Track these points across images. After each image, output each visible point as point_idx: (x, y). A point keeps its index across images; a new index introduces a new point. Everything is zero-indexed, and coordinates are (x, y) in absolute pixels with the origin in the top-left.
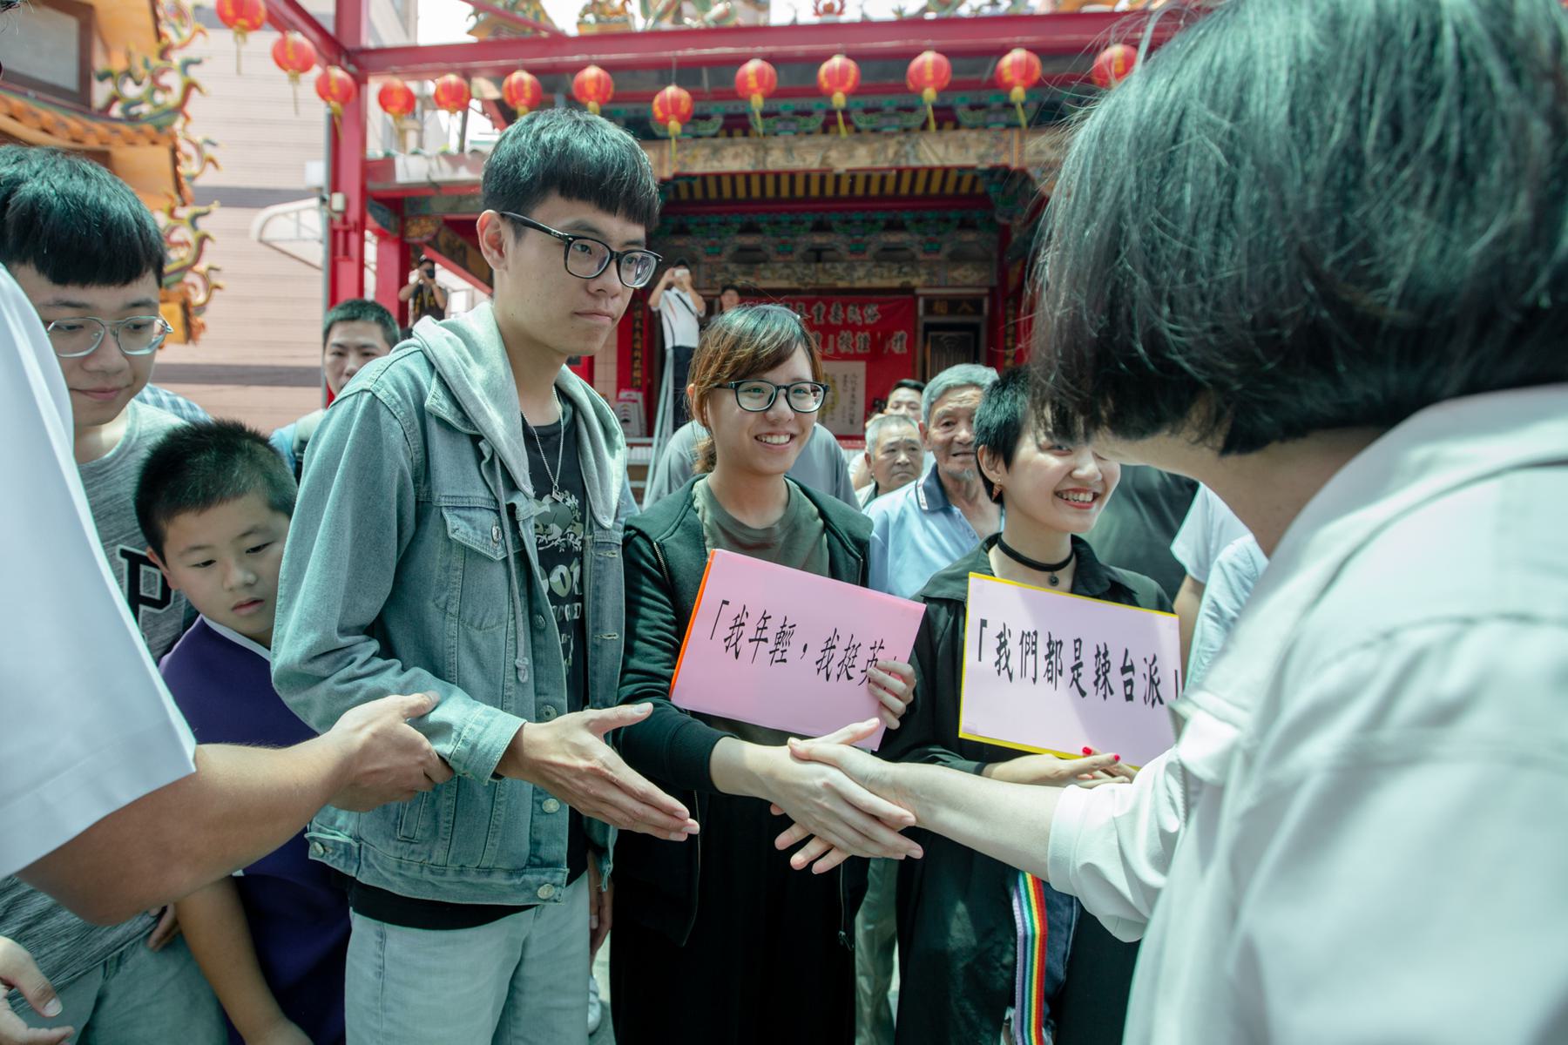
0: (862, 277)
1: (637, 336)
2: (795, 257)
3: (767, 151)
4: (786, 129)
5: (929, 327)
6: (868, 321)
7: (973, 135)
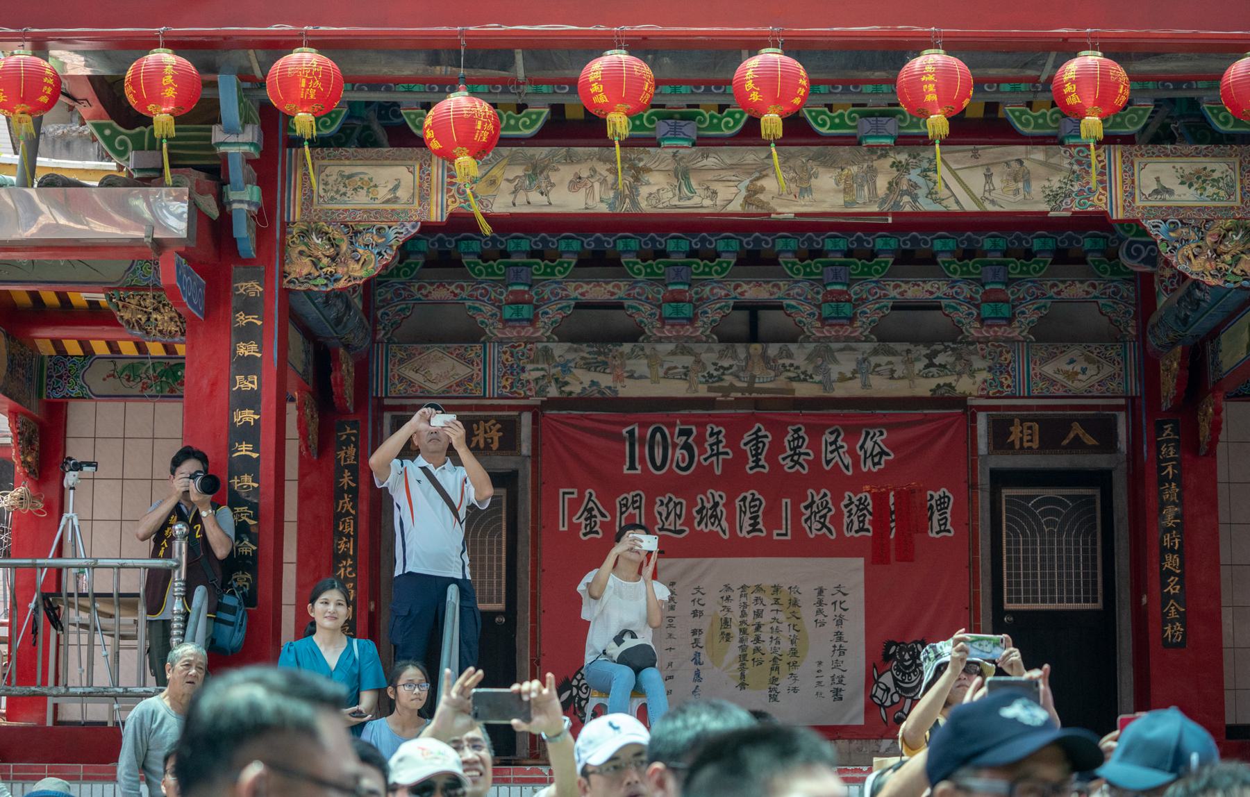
0: (848, 374)
1: (346, 503)
2: (701, 328)
3: (638, 174)
4: (675, 134)
5: (1000, 478)
6: (868, 466)
7: (1038, 154)
